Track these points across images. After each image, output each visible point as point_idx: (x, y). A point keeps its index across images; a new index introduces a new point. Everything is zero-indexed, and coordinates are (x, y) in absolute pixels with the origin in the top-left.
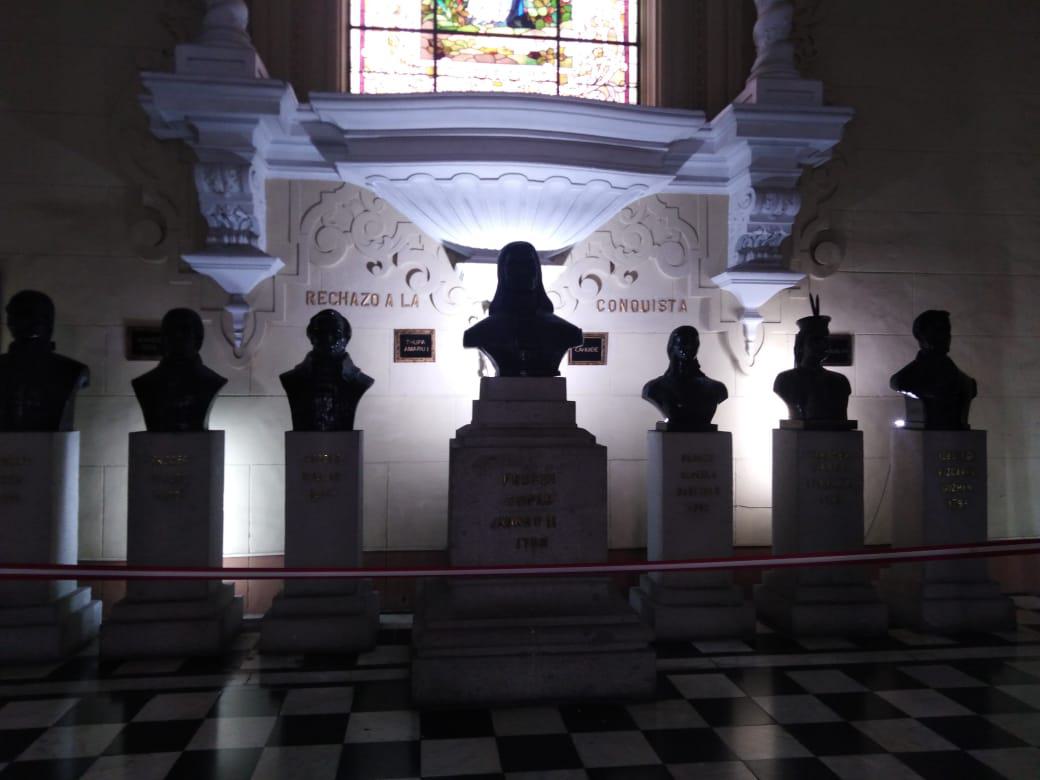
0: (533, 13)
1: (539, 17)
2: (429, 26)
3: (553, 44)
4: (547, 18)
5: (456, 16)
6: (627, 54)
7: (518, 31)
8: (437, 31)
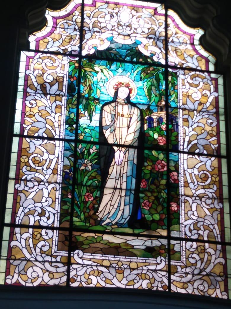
0: (148, 217)
1: (153, 221)
2: (67, 225)
3: (165, 242)
4: (159, 224)
5: (87, 219)
6: (22, 129)
7: (137, 231)
8: (73, 228)
